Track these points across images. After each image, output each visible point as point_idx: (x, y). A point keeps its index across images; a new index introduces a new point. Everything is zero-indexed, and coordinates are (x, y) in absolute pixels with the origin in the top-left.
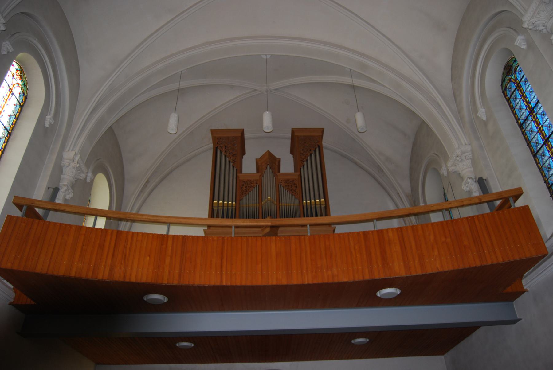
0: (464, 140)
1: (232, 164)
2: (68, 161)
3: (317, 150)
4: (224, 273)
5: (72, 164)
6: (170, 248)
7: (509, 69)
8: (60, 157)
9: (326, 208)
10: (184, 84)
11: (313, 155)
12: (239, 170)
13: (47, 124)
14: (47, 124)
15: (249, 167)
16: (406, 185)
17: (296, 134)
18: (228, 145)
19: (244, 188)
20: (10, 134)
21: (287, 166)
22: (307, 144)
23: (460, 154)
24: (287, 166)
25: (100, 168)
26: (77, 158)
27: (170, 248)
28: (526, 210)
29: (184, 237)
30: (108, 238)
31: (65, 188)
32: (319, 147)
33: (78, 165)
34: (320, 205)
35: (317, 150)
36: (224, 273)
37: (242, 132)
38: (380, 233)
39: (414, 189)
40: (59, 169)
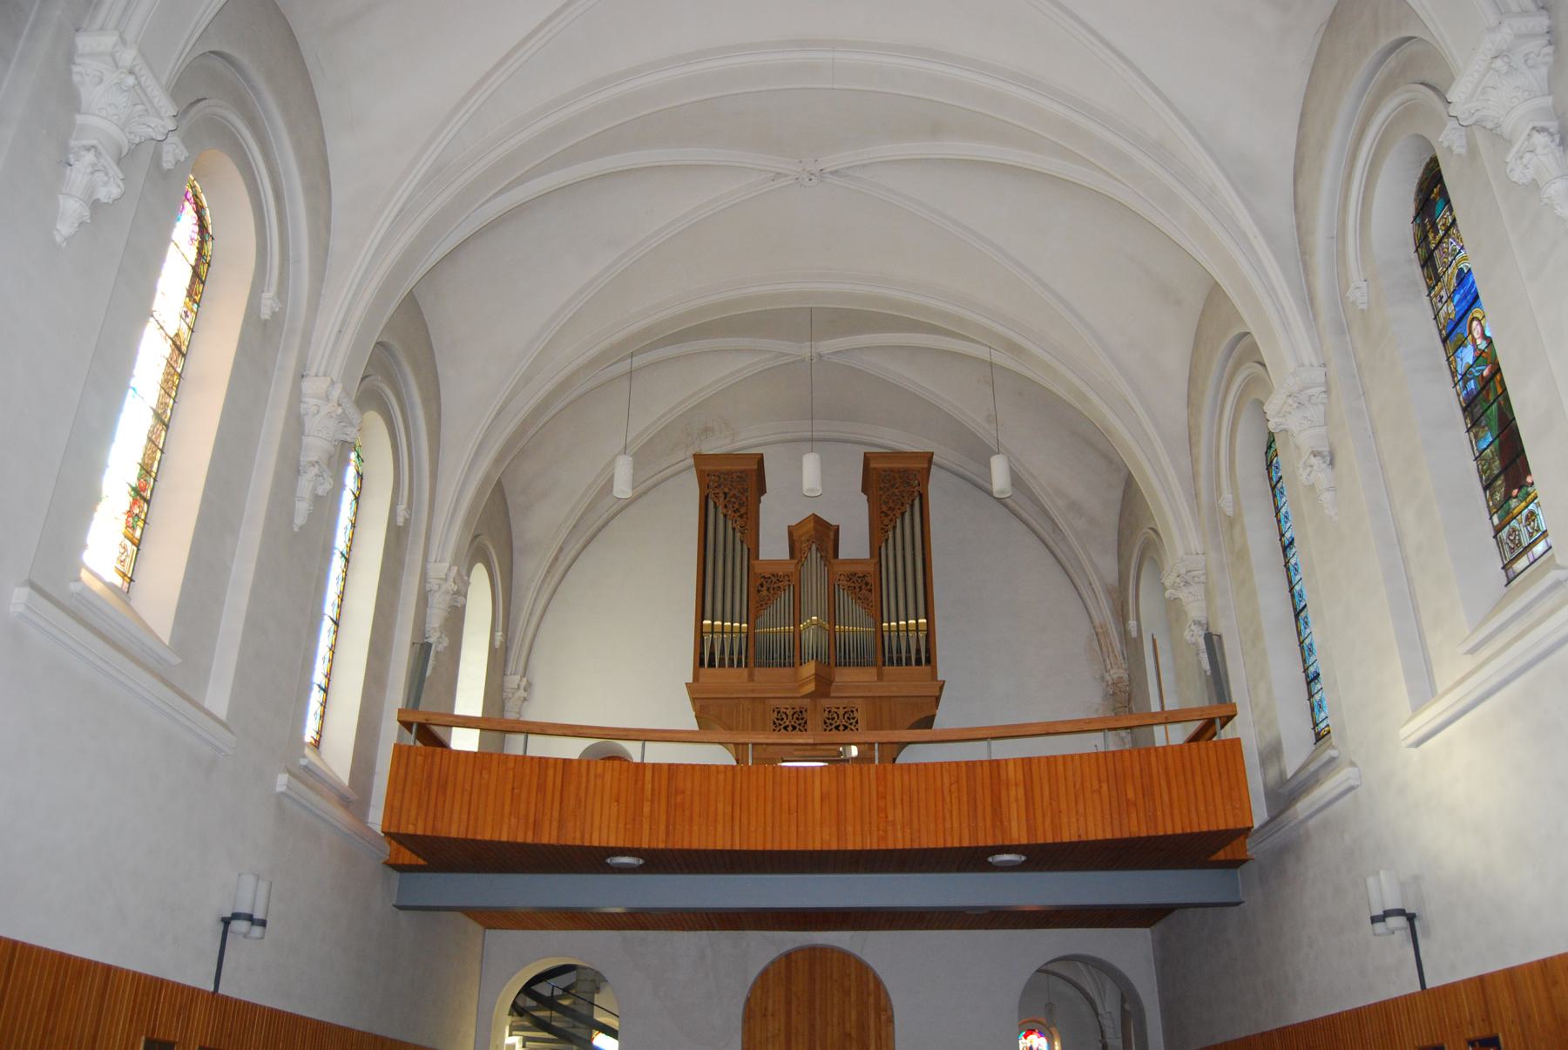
0: (1195, 544)
1: (738, 535)
2: (315, 401)
3: (917, 503)
4: (737, 828)
5: (325, 409)
6: (648, 787)
7: (1431, 192)
8: (297, 395)
9: (927, 636)
10: (638, 361)
11: (907, 516)
12: (754, 551)
13: (266, 313)
14: (266, 313)
15: (773, 547)
16: (1108, 565)
17: (873, 465)
18: (731, 489)
19: (764, 593)
20: (347, 560)
21: (855, 544)
22: (896, 487)
23: (1183, 571)
24: (855, 544)
25: (477, 553)
26: (337, 392)
27: (648, 787)
28: (1236, 743)
29: (672, 767)
30: (551, 772)
31: (315, 470)
32: (921, 496)
33: (340, 411)
34: (917, 630)
35: (917, 503)
36: (737, 828)
37: (760, 460)
38: (996, 765)
39: (1122, 578)
40: (296, 425)
